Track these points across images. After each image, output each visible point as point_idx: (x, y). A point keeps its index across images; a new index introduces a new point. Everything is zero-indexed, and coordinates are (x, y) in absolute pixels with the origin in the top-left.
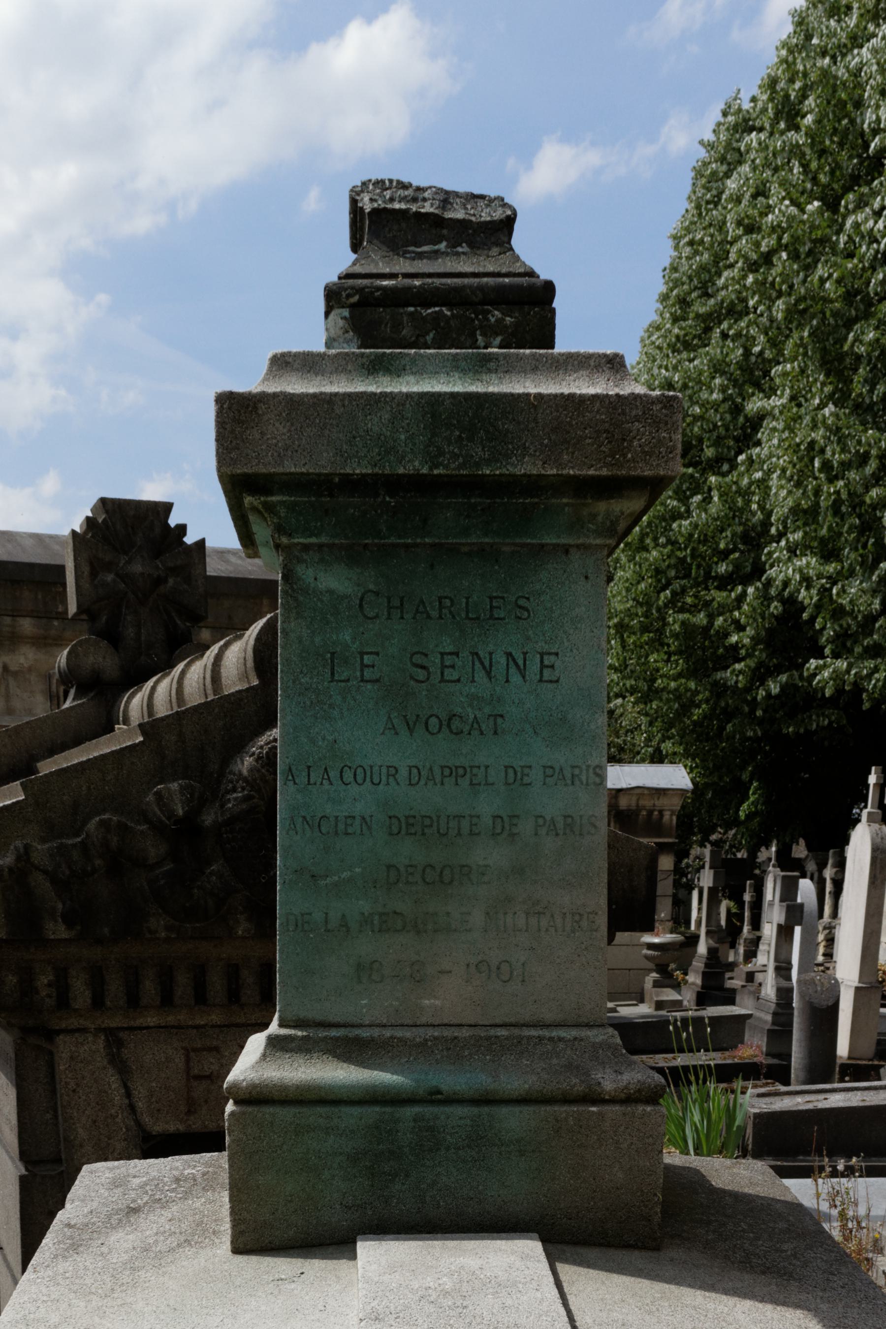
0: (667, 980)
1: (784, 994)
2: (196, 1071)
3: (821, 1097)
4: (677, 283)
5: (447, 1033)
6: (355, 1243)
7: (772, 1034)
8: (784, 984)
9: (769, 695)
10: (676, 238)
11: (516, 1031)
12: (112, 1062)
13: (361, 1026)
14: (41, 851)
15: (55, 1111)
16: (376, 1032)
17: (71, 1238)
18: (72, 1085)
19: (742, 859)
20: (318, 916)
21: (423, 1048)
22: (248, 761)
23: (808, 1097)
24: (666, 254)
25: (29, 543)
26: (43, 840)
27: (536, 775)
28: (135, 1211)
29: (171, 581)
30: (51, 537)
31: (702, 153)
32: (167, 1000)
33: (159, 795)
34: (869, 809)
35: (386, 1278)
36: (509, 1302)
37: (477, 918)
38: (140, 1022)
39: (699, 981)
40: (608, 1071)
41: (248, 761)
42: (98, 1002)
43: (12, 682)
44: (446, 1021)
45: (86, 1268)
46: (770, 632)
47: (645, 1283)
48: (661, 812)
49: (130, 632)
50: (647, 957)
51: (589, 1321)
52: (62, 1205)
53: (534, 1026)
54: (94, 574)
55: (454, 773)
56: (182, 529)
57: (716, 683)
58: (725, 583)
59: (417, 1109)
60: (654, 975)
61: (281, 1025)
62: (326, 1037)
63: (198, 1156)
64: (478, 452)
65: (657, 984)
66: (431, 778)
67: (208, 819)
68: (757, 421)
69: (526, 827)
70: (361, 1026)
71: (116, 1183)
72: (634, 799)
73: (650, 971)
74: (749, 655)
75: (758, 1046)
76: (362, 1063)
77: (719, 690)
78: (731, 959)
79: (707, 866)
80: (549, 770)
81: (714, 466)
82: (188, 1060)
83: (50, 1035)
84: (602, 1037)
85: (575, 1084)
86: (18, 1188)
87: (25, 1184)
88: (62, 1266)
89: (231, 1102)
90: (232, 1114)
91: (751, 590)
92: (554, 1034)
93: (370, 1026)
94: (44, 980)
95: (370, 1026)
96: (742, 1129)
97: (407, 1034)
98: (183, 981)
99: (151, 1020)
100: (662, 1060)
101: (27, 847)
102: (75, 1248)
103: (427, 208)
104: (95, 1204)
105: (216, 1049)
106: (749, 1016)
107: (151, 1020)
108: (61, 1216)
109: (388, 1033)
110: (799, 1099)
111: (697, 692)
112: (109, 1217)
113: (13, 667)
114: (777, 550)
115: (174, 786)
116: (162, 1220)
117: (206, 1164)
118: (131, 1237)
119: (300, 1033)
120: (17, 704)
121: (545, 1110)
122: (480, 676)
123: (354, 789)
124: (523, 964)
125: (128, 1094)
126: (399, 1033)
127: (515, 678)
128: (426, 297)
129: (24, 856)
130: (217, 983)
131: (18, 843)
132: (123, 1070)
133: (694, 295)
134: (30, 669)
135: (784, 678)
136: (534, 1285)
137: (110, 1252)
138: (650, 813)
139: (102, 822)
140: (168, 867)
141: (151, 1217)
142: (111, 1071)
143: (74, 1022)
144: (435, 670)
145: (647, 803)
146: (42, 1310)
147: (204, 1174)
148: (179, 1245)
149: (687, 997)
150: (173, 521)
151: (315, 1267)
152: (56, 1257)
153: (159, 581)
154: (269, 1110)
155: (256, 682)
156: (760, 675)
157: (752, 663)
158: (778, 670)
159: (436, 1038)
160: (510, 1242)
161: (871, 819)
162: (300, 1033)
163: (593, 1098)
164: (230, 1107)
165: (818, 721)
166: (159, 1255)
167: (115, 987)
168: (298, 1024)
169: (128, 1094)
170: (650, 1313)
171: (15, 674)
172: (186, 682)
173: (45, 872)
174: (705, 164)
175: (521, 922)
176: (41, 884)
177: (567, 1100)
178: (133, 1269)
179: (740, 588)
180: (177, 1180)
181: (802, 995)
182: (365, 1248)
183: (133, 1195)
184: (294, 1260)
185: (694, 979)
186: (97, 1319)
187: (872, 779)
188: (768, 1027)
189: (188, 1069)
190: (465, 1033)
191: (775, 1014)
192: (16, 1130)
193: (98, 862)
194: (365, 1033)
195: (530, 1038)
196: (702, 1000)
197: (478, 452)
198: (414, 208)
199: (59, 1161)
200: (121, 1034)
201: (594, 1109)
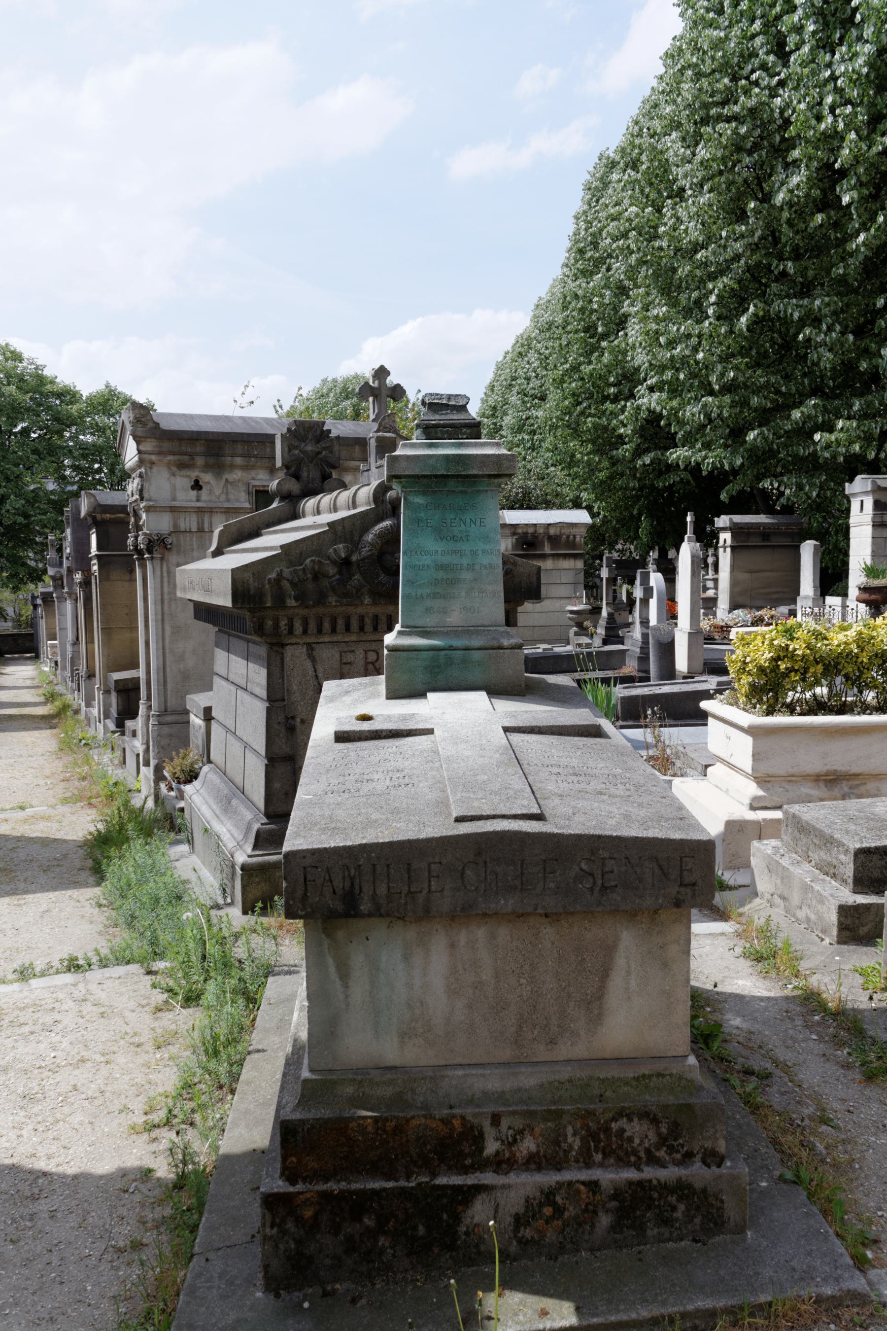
0: (582, 630)
1: (645, 636)
2: (344, 661)
3: (658, 688)
4: (577, 242)
5: (455, 629)
7: (640, 659)
8: (645, 631)
9: (644, 464)
10: (577, 218)
12: (309, 657)
14: (287, 572)
15: (283, 679)
18: (292, 667)
20: (414, 594)
21: (447, 634)
22: (371, 536)
23: (650, 688)
24: (570, 228)
25: (239, 422)
26: (288, 568)
27: (480, 552)
29: (324, 453)
30: (249, 418)
31: (588, 177)
32: (334, 630)
33: (335, 550)
34: (688, 535)
37: (463, 594)
38: (321, 640)
39: (603, 633)
41: (371, 536)
42: (305, 632)
43: (229, 487)
46: (642, 427)
48: (574, 536)
49: (305, 474)
50: (569, 618)
54: (290, 451)
55: (455, 552)
56: (329, 431)
57: (612, 458)
58: (615, 399)
60: (575, 628)
64: (460, 468)
65: (576, 634)
66: (448, 553)
67: (354, 558)
68: (625, 318)
69: (477, 567)
72: (558, 529)
73: (573, 626)
74: (630, 442)
75: (633, 667)
76: (428, 638)
77: (614, 462)
78: (630, 620)
79: (604, 565)
80: (484, 551)
81: (604, 336)
82: (341, 656)
83: (283, 645)
85: (495, 643)
91: (629, 404)
94: (283, 623)
96: (615, 706)
97: (442, 629)
98: (341, 623)
99: (326, 639)
100: (577, 676)
101: (281, 571)
103: (444, 402)
105: (353, 651)
106: (628, 650)
107: (326, 639)
110: (646, 689)
111: (600, 462)
113: (230, 480)
114: (641, 389)
115: (341, 546)
120: (231, 497)
121: (486, 651)
122: (462, 525)
123: (425, 557)
125: (315, 671)
127: (473, 525)
128: (444, 426)
129: (280, 574)
130: (355, 624)
131: (278, 569)
132: (313, 660)
133: (588, 248)
134: (239, 481)
135: (652, 455)
138: (568, 536)
139: (312, 561)
140: (337, 577)
142: (308, 661)
143: (294, 640)
144: (449, 523)
145: (566, 531)
149: (597, 642)
150: (325, 428)
153: (319, 453)
154: (398, 653)
155: (373, 506)
156: (638, 452)
157: (633, 445)
158: (647, 451)
161: (690, 540)
165: (673, 478)
167: (312, 626)
168: (407, 627)
169: (315, 671)
171: (231, 483)
172: (338, 500)
173: (288, 580)
174: (583, 197)
175: (477, 594)
176: (286, 584)
179: (623, 403)
181: (653, 637)
182: (430, 695)
185: (601, 631)
187: (689, 519)
188: (638, 655)
189: (341, 660)
191: (641, 648)
193: (309, 576)
194: (428, 629)
196: (605, 642)
197: (460, 468)
198: (440, 401)
199: (283, 700)
200: (314, 646)
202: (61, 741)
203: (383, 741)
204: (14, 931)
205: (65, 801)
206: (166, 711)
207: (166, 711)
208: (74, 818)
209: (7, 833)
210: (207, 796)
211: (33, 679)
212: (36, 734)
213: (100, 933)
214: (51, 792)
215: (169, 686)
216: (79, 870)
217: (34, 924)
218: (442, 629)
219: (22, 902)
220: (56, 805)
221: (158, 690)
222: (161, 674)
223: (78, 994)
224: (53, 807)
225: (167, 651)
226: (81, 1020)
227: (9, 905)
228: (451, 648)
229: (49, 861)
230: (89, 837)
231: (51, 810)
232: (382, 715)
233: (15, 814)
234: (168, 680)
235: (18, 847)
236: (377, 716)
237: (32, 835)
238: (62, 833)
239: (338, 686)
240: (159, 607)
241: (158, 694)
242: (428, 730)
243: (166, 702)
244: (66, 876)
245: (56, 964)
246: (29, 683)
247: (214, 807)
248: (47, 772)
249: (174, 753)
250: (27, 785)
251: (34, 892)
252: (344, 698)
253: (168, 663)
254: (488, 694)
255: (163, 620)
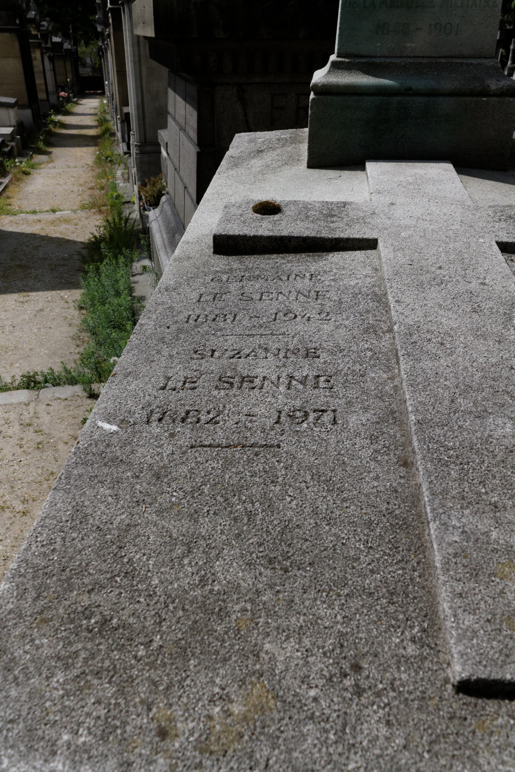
5: (417, 60)
6: (365, 164)
11: (450, 60)
13: (376, 57)
16: (383, 60)
17: (233, 161)
19: (510, 29)
28: (262, 151)
35: (381, 177)
36: (440, 188)
40: (493, 80)
44: (416, 55)
45: (242, 173)
47: (502, 184)
51: (477, 198)
52: (227, 149)
53: (459, 58)
59: (399, 98)
61: (338, 57)
62: (359, 62)
63: (287, 131)
70: (376, 57)
71: (250, 141)
84: (491, 63)
86: (196, 158)
87: (199, 156)
88: (231, 172)
89: (312, 93)
90: (313, 99)
92: (469, 61)
93: (380, 57)
95: (380, 57)
97: (398, 61)
102: (236, 165)
104: (243, 149)
108: (227, 153)
109: (388, 61)
112: (250, 154)
116: (274, 155)
117: (291, 134)
118: (260, 161)
119: (347, 60)
124: (458, 25)
125: (246, 115)
126: (394, 60)
136: (451, 181)
137: (252, 167)
141: (268, 154)
146: (224, 189)
147: (290, 138)
148: (282, 165)
151: (346, 174)
152: (228, 169)
154: (330, 98)
159: (411, 63)
160: (437, 164)
162: (347, 60)
163: (485, 93)
164: (312, 96)
166: (274, 169)
169: (246, 115)
170: (505, 196)
177: (472, 94)
178: (263, 174)
180: (278, 140)
182: (370, 166)
183: (259, 145)
184: (336, 171)
186: (249, 193)
190: (425, 61)
192: (196, 132)
194: (378, 60)
195: (457, 63)
201: (484, 99)
202: (99, 158)
203: (291, 257)
204: (11, 328)
205: (83, 207)
206: (146, 141)
207: (146, 141)
208: (86, 222)
209: (37, 232)
210: (161, 225)
211: (95, 109)
212: (85, 149)
213: (73, 338)
214: (80, 197)
215: (147, 120)
216: (77, 270)
217: (28, 323)
218: (398, 61)
219: (27, 299)
220: (77, 210)
221: (139, 124)
222: (141, 110)
223: (26, 417)
224: (75, 211)
225: (145, 90)
226: (19, 451)
227: (16, 301)
228: (409, 92)
229: (58, 260)
230: (93, 240)
231: (73, 214)
232: (295, 203)
233: (47, 216)
234: (146, 115)
235: (40, 246)
236: (288, 204)
237: (54, 236)
238: (75, 235)
239: (250, 141)
240: (136, 49)
241: (139, 127)
242: (367, 240)
243: (145, 135)
244: (66, 275)
245: (18, 379)
246: (92, 111)
247: (165, 236)
248: (82, 181)
249: (147, 180)
250: (66, 190)
251: (38, 290)
252: (253, 162)
253: (145, 101)
254: (455, 166)
255: (140, 61)
